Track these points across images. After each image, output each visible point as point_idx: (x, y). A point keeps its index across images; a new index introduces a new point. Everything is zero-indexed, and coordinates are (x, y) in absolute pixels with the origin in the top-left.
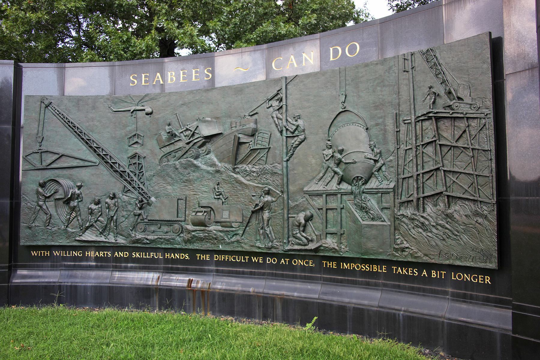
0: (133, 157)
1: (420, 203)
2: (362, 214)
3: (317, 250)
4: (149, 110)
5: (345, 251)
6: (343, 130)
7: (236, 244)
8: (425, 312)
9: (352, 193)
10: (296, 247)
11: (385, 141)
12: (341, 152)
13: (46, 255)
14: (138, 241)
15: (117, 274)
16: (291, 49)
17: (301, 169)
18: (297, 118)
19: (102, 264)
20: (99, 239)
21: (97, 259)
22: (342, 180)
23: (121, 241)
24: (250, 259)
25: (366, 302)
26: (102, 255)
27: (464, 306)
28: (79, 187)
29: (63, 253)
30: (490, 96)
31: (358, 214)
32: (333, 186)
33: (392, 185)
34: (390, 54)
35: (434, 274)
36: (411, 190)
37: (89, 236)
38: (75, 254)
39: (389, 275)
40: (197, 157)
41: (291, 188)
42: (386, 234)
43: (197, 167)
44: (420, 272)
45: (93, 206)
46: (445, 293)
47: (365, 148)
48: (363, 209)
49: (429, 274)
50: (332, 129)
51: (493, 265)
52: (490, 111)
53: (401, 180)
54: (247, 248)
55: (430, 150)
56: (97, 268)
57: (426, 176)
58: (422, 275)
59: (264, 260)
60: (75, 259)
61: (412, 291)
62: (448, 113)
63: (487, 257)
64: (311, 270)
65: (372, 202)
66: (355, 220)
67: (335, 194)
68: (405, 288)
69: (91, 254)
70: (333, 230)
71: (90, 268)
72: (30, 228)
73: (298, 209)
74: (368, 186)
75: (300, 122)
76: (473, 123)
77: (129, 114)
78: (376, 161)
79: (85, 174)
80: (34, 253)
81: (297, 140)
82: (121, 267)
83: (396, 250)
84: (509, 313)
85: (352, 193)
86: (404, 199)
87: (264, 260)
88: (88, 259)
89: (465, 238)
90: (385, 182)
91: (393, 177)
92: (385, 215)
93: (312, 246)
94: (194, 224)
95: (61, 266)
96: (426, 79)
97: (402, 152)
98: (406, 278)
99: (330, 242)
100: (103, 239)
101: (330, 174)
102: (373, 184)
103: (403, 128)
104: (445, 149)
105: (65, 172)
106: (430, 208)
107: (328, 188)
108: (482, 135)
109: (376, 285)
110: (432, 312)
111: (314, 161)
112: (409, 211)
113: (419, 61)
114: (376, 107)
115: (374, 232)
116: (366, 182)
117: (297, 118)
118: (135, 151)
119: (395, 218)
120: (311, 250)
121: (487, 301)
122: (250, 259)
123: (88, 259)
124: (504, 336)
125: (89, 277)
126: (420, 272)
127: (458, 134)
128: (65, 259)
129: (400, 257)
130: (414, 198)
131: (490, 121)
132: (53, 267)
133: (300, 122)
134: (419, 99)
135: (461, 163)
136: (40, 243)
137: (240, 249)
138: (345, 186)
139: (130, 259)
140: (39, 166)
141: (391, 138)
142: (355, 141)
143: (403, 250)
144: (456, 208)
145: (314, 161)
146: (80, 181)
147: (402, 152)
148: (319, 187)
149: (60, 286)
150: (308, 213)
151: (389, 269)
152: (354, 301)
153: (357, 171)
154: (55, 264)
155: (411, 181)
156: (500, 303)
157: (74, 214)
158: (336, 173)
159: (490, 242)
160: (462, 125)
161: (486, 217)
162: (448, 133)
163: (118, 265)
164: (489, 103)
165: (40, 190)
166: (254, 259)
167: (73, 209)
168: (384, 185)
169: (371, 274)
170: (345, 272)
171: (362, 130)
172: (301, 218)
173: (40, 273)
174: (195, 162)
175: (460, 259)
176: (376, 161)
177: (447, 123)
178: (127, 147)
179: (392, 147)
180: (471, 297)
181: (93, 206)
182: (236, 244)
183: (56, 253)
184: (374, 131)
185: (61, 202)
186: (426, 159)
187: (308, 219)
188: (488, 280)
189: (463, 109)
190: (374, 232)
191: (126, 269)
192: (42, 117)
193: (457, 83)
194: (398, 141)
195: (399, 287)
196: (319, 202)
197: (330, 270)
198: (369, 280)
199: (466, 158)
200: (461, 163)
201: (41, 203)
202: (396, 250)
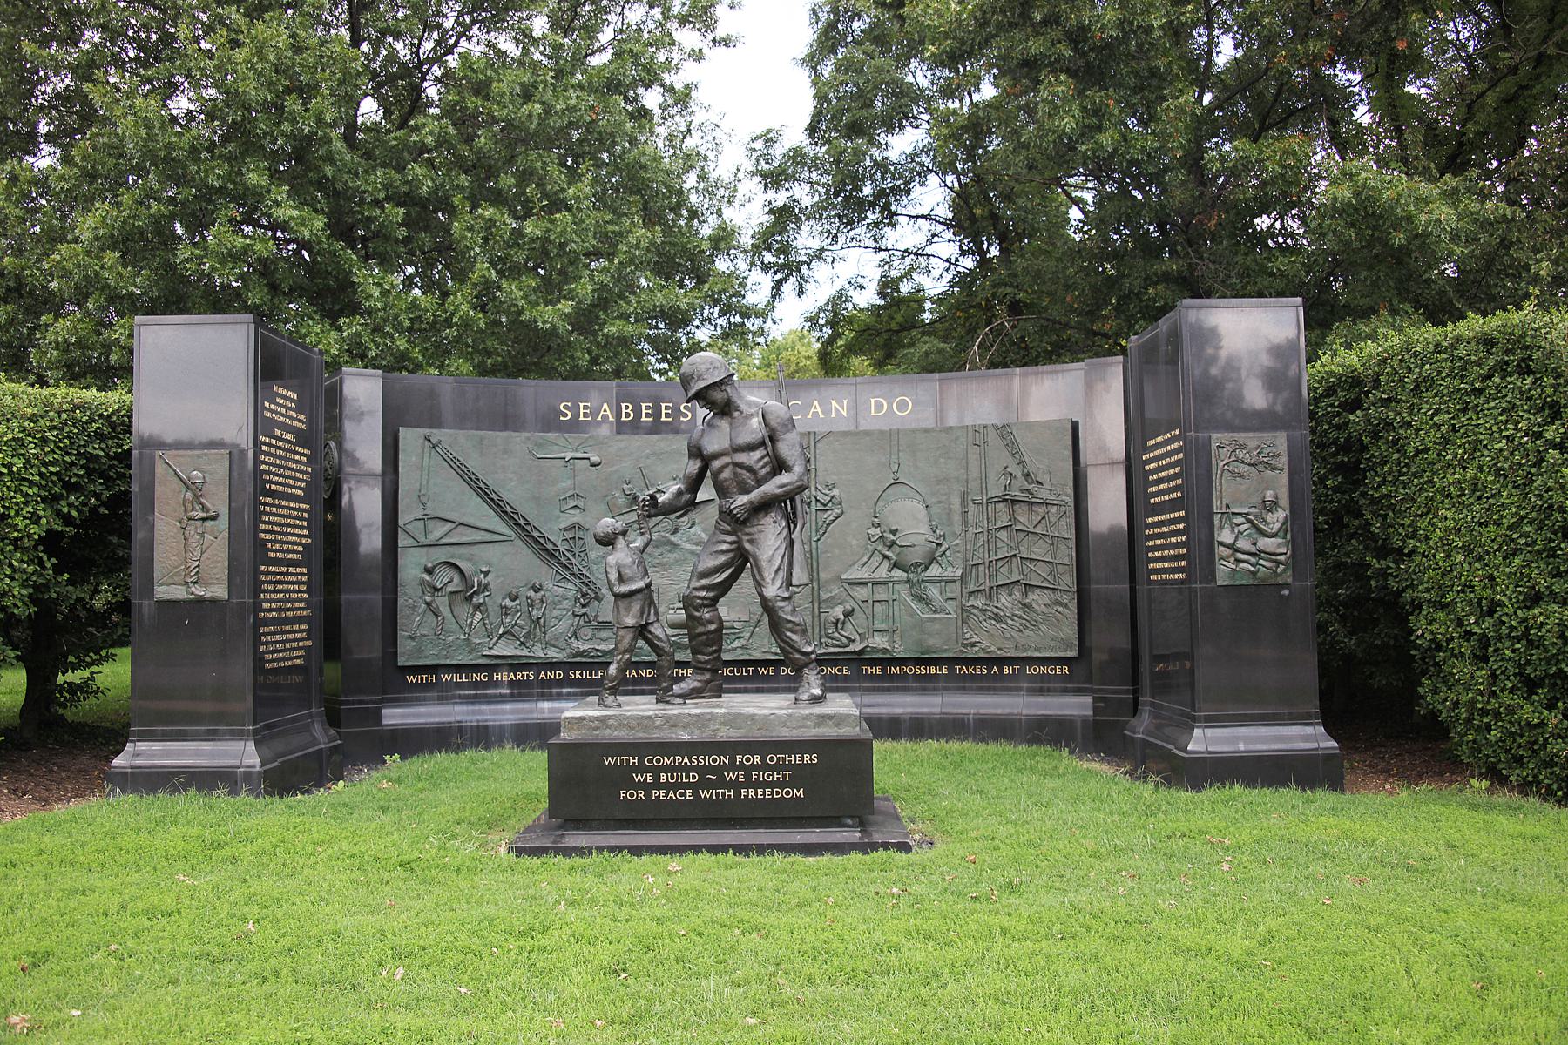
0: (572, 527)
1: (992, 593)
2: (920, 606)
3: (862, 651)
4: (594, 459)
5: (900, 651)
6: (895, 506)
7: (739, 652)
8: (999, 711)
9: (908, 581)
10: (832, 650)
11: (950, 522)
12: (894, 532)
13: (431, 679)
14: (581, 654)
15: (546, 705)
16: (814, 392)
17: (837, 551)
18: (831, 487)
19: (521, 691)
20: (519, 652)
21: (512, 684)
22: (896, 565)
23: (554, 654)
24: (755, 671)
25: (925, 710)
26: (519, 676)
27: (1041, 699)
28: (486, 574)
29: (456, 678)
30: (1071, 484)
31: (915, 606)
32: (883, 573)
33: (959, 573)
34: (952, 420)
35: (1006, 669)
36: (981, 578)
37: (504, 649)
38: (479, 676)
39: (952, 676)
40: (675, 532)
41: (823, 575)
42: (953, 628)
43: (675, 546)
44: (990, 670)
45: (507, 602)
46: (1020, 689)
47: (924, 529)
48: (923, 600)
49: (1001, 670)
50: (880, 503)
51: (1073, 653)
52: (1071, 499)
53: (969, 568)
54: (758, 655)
55: (1003, 535)
56: (512, 698)
57: (1000, 564)
58: (992, 670)
59: (777, 671)
60: (476, 685)
61: (981, 690)
62: (1026, 497)
63: (1066, 645)
64: (846, 678)
65: (934, 592)
66: (913, 614)
67: (885, 583)
68: (971, 689)
69: (503, 676)
70: (883, 626)
71: (501, 699)
72: (412, 638)
73: (833, 602)
74: (928, 573)
75: (835, 492)
76: (1053, 510)
77: (562, 462)
78: (939, 545)
79: (491, 553)
80: (411, 679)
81: (832, 515)
82: (551, 694)
83: (965, 646)
84: (1089, 700)
85: (908, 581)
86: (973, 588)
87: (777, 671)
88: (497, 684)
89: (1044, 628)
90: (950, 569)
91: (959, 563)
92: (951, 607)
93: (857, 647)
94: (672, 626)
95: (454, 697)
96: (1000, 458)
97: (970, 535)
98: (973, 677)
99: (879, 641)
100: (525, 652)
101: (878, 558)
102: (934, 570)
103: (972, 508)
104: (1021, 535)
105: (462, 550)
106: (1004, 599)
107: (876, 575)
108: (1063, 523)
109: (935, 689)
110: (1007, 711)
111: (854, 542)
112: (980, 602)
113: (992, 436)
114: (939, 482)
115: (937, 626)
116: (926, 568)
117: (831, 487)
118: (575, 520)
119: (964, 610)
120: (855, 652)
121: (1065, 691)
122: (755, 671)
123: (497, 684)
124: (1085, 721)
125: (504, 712)
126: (990, 670)
127: (1036, 519)
128: (459, 686)
129: (970, 653)
130: (986, 587)
131: (1071, 509)
132: (442, 700)
133: (835, 492)
134: (992, 477)
135: (1039, 550)
136: (428, 662)
137: (746, 657)
138: (898, 574)
139: (566, 682)
140: (423, 540)
141: (957, 518)
142: (912, 522)
143: (973, 645)
144: (1033, 597)
145: (854, 542)
146: (488, 564)
147: (970, 535)
148: (864, 574)
149: (460, 728)
150: (849, 607)
151: (951, 670)
152: (909, 710)
153: (915, 556)
154: (445, 694)
155: (981, 568)
156: (1079, 691)
157: (479, 616)
158: (885, 557)
159: (1070, 631)
160: (1041, 510)
161: (1066, 606)
162: (1024, 517)
163: (545, 690)
164: (1071, 492)
165: (426, 577)
166: (762, 671)
167: (477, 607)
168: (950, 572)
169: (928, 677)
170: (893, 677)
171: (921, 507)
172: (838, 612)
173: (422, 709)
174: (673, 538)
175: (1038, 650)
176: (939, 545)
177: (1025, 507)
178: (557, 513)
179: (958, 529)
180: (1049, 690)
181: (507, 602)
182: (739, 652)
183: (446, 678)
184: (935, 510)
185: (458, 598)
186: (999, 544)
187: (847, 614)
188: (1065, 670)
189: (1042, 494)
190: (937, 626)
191: (559, 697)
192: (425, 463)
193: (1036, 465)
194: (965, 523)
195: (964, 689)
196: (861, 593)
197: (873, 677)
198: (926, 684)
199: (1045, 546)
200: (1039, 550)
201: (428, 599)
202: (965, 646)
